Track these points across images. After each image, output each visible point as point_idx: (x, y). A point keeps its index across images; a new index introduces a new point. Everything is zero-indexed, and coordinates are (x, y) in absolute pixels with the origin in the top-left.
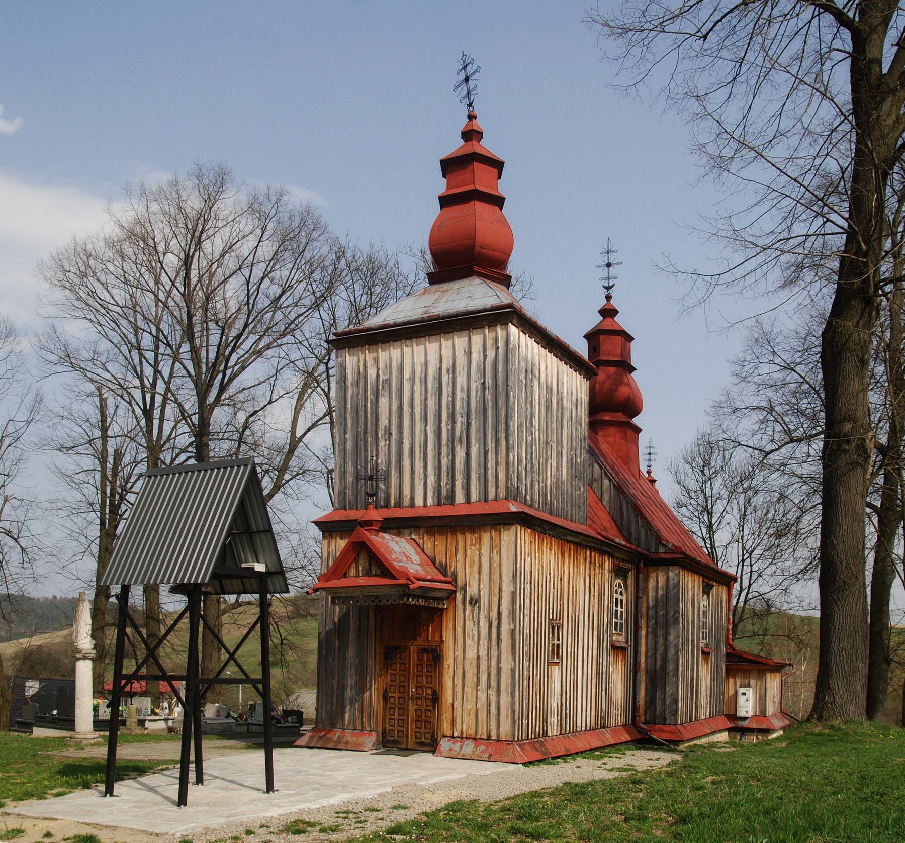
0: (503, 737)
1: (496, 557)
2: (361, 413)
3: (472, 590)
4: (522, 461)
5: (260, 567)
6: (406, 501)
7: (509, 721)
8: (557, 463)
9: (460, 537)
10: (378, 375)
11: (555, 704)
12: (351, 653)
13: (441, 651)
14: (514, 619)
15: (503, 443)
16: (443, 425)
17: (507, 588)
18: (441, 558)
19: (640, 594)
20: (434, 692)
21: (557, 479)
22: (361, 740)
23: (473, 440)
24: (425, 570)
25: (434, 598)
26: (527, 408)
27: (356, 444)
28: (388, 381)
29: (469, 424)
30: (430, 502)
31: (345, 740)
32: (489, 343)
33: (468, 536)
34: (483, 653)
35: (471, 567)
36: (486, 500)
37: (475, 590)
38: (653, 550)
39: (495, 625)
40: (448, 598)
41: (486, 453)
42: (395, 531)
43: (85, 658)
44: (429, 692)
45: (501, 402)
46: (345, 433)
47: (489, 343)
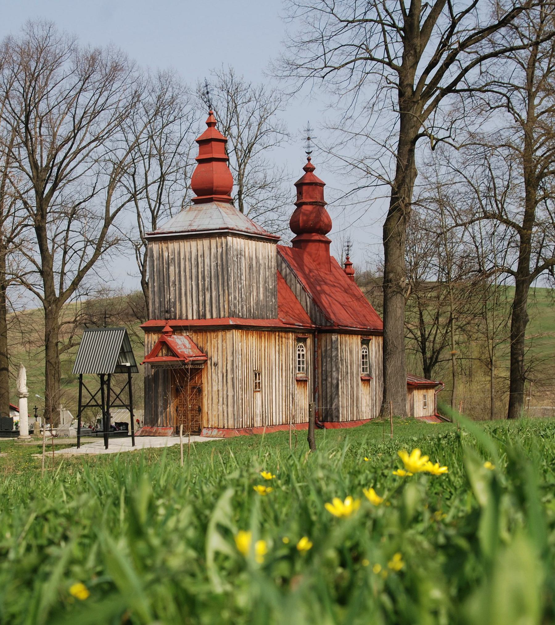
0: (230, 427)
1: (224, 345)
2: (161, 273)
3: (214, 360)
4: (236, 298)
5: (128, 364)
6: (184, 317)
7: (232, 419)
8: (257, 293)
9: (208, 334)
10: (168, 256)
11: (258, 411)
12: (160, 389)
13: (202, 387)
14: (233, 372)
15: (226, 291)
16: (200, 282)
17: (230, 359)
18: (200, 344)
19: (316, 350)
20: (199, 407)
21: (257, 301)
22: (166, 431)
23: (213, 290)
24: (193, 351)
25: (197, 364)
26: (238, 272)
27: (160, 288)
28: (173, 259)
29: (211, 282)
30: (195, 317)
31: (158, 432)
32: (219, 244)
33: (212, 334)
34: (220, 388)
35: (214, 348)
36: (220, 317)
37: (216, 360)
38: (324, 324)
39: (225, 376)
40: (204, 363)
41: (219, 296)
42: (179, 331)
43: (24, 397)
44: (197, 407)
45: (225, 273)
46: (154, 283)
47: (219, 244)
